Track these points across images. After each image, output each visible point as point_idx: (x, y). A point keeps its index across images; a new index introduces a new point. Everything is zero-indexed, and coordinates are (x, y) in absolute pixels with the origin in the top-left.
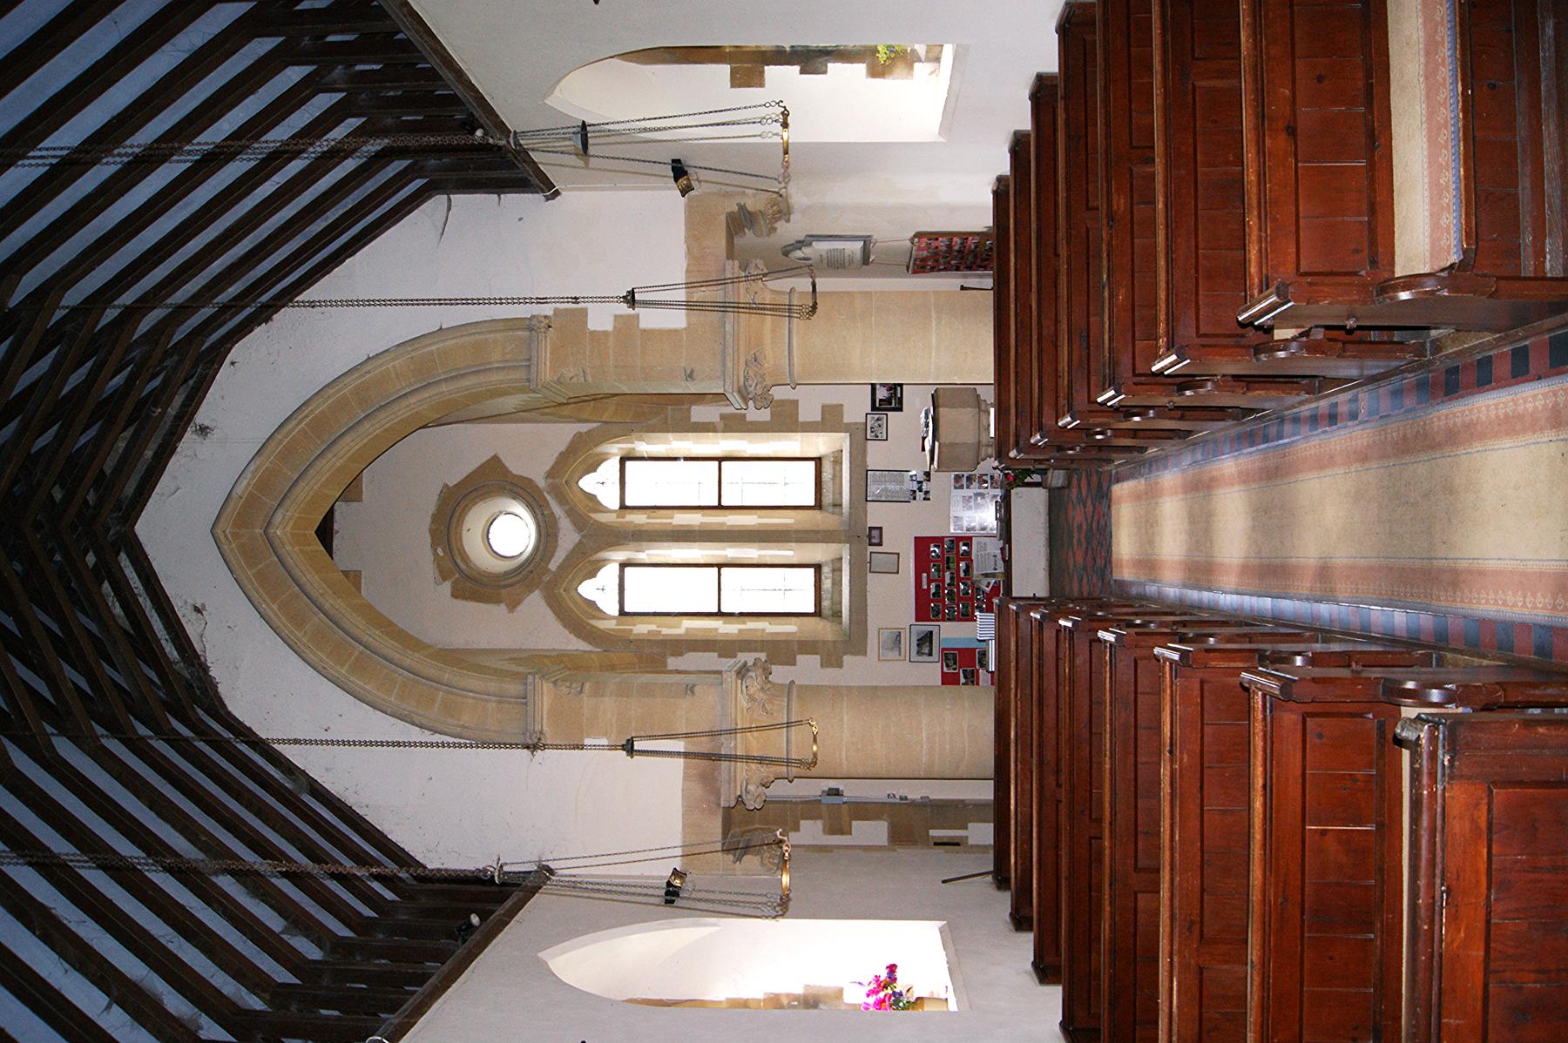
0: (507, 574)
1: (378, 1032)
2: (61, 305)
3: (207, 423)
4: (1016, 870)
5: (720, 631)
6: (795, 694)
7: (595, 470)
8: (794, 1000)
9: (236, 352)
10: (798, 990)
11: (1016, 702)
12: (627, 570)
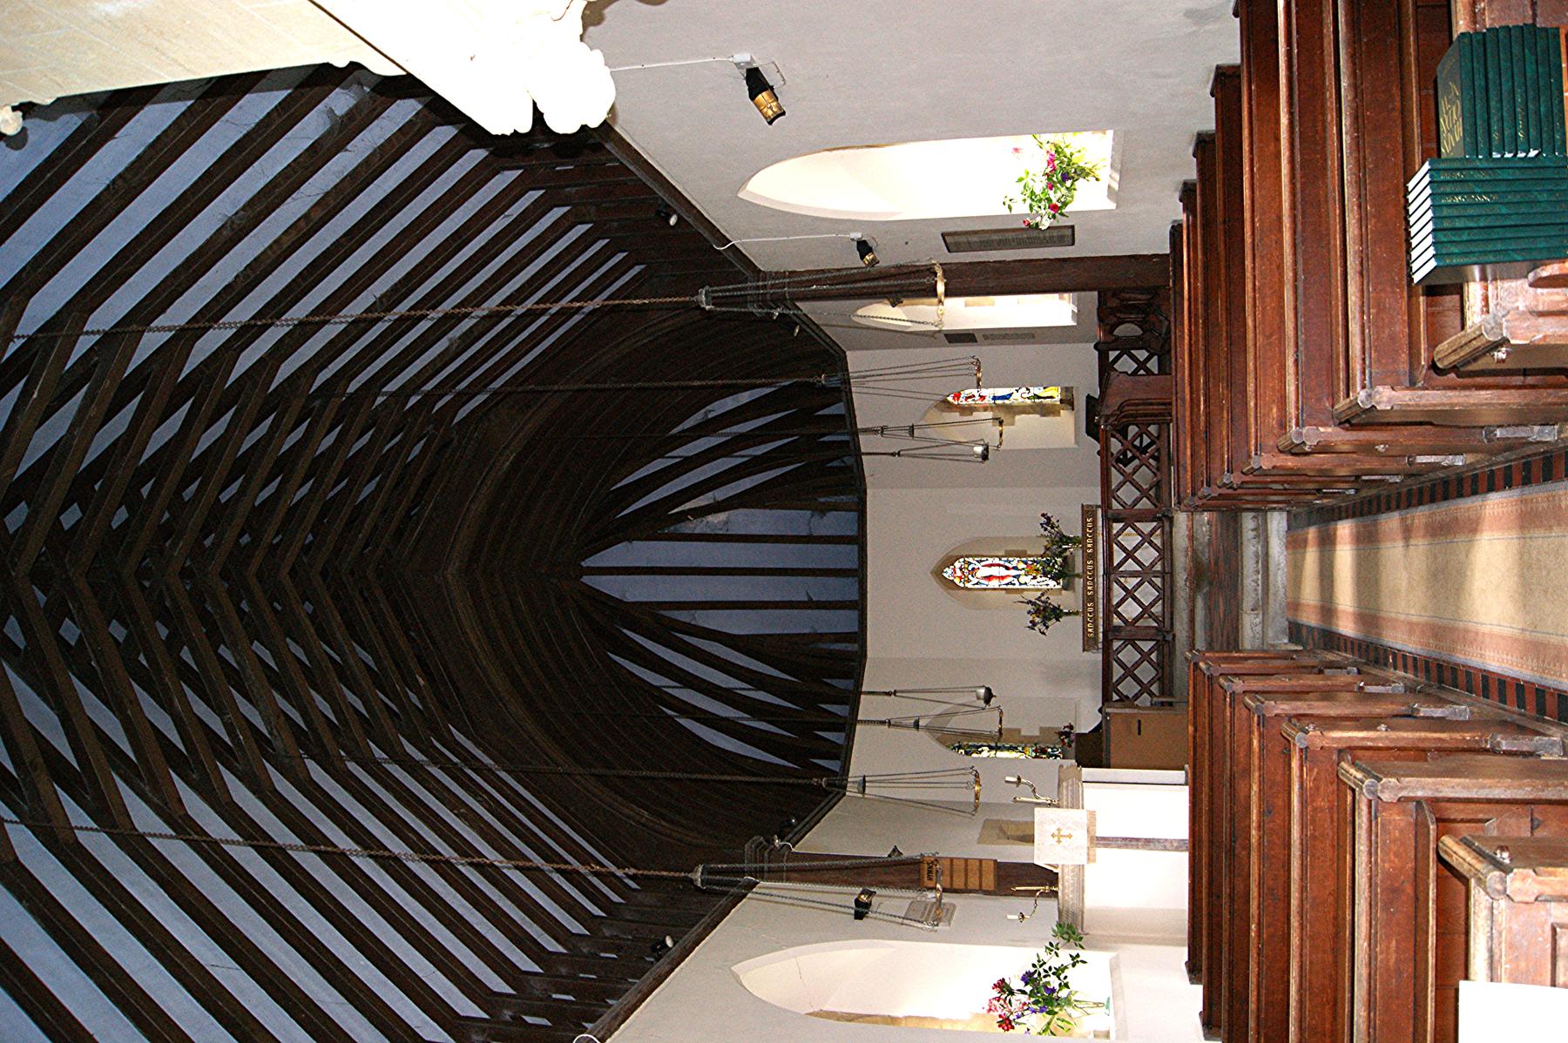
2: (85, 330)
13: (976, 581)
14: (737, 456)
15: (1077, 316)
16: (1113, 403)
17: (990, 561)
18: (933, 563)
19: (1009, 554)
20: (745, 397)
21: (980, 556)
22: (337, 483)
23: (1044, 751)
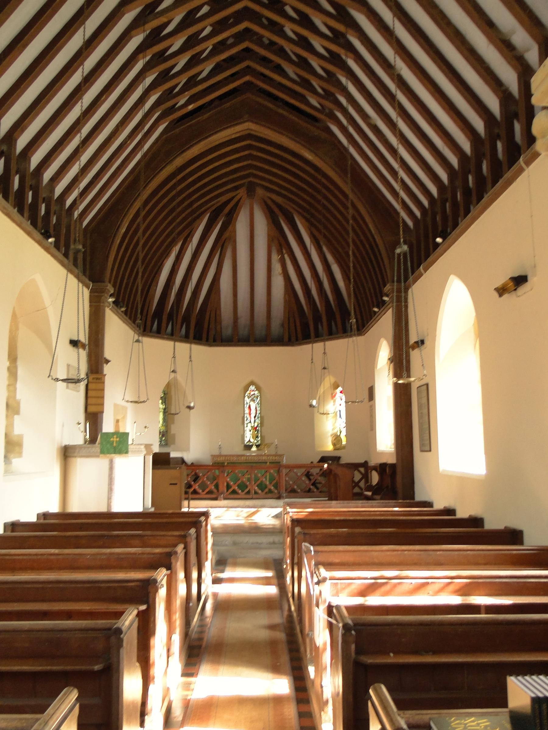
13: (248, 402)
14: (311, 250)
15: (382, 453)
16: (339, 471)
17: (258, 409)
18: (257, 381)
19: (262, 418)
20: (341, 284)
21: (261, 404)
22: (295, 54)
23: (163, 436)
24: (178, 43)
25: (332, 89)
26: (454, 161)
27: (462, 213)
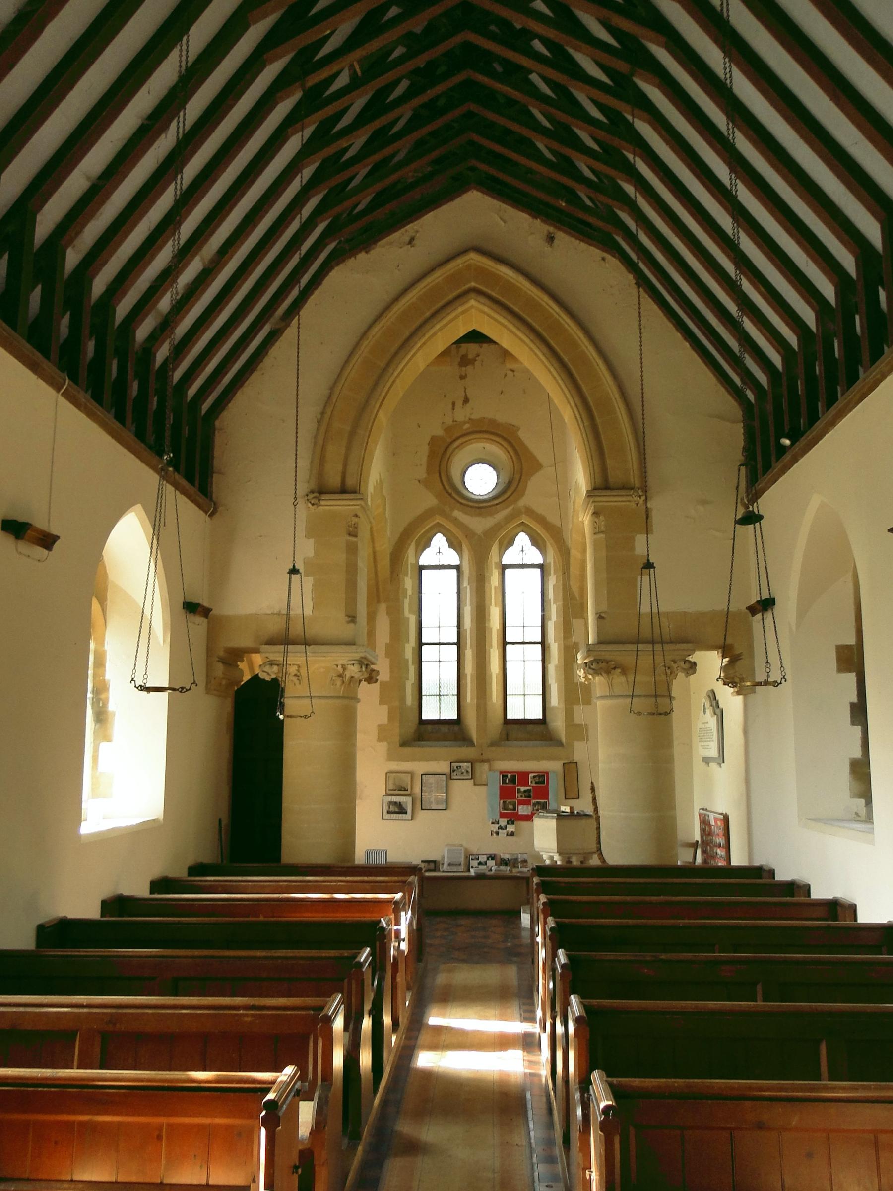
0: (449, 479)
1: (71, 383)
3: (556, 241)
4: (201, 881)
5: (407, 645)
6: (346, 702)
7: (533, 545)
8: (103, 703)
9: (613, 262)
10: (111, 707)
11: (335, 882)
12: (455, 571)
24: (359, 141)
25: (616, 142)
26: (848, 261)
27: (866, 356)
